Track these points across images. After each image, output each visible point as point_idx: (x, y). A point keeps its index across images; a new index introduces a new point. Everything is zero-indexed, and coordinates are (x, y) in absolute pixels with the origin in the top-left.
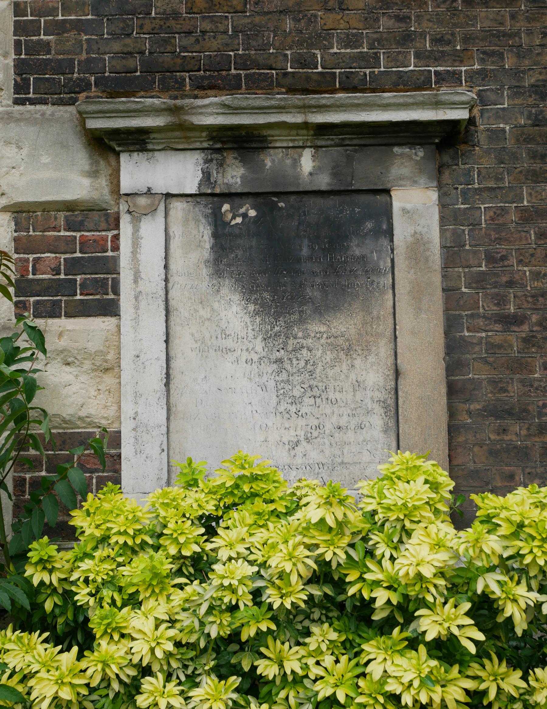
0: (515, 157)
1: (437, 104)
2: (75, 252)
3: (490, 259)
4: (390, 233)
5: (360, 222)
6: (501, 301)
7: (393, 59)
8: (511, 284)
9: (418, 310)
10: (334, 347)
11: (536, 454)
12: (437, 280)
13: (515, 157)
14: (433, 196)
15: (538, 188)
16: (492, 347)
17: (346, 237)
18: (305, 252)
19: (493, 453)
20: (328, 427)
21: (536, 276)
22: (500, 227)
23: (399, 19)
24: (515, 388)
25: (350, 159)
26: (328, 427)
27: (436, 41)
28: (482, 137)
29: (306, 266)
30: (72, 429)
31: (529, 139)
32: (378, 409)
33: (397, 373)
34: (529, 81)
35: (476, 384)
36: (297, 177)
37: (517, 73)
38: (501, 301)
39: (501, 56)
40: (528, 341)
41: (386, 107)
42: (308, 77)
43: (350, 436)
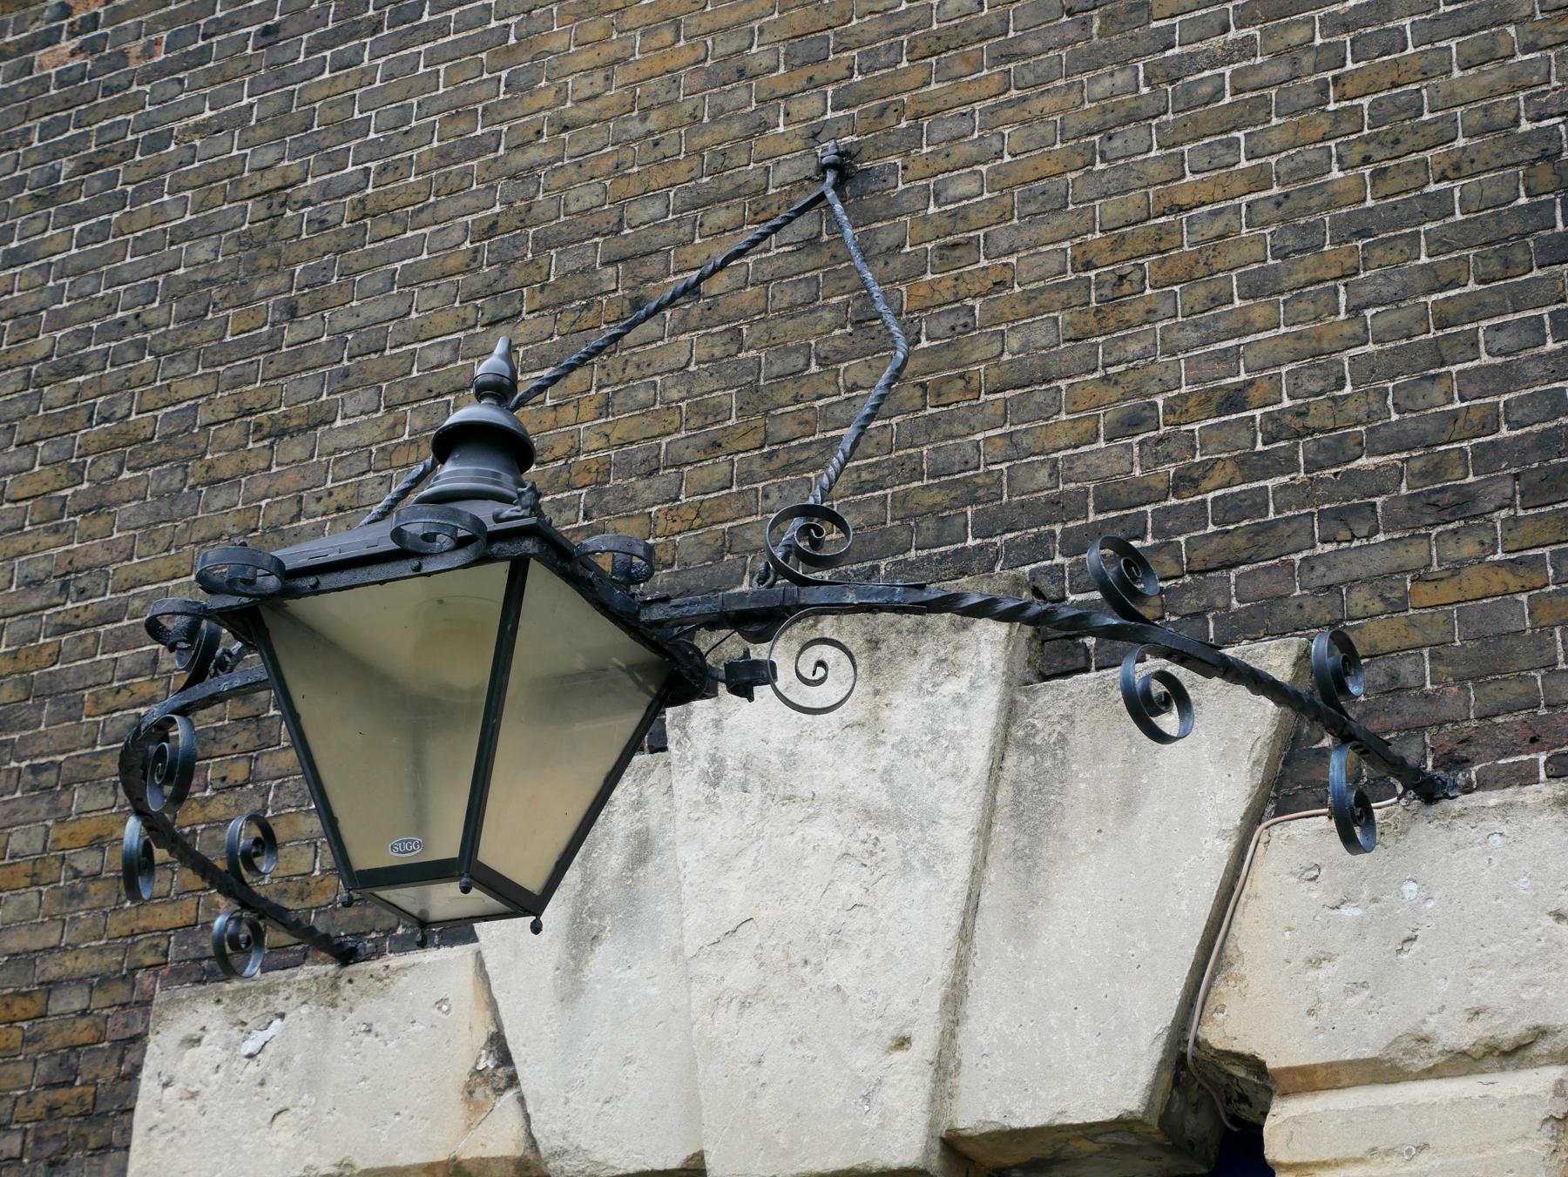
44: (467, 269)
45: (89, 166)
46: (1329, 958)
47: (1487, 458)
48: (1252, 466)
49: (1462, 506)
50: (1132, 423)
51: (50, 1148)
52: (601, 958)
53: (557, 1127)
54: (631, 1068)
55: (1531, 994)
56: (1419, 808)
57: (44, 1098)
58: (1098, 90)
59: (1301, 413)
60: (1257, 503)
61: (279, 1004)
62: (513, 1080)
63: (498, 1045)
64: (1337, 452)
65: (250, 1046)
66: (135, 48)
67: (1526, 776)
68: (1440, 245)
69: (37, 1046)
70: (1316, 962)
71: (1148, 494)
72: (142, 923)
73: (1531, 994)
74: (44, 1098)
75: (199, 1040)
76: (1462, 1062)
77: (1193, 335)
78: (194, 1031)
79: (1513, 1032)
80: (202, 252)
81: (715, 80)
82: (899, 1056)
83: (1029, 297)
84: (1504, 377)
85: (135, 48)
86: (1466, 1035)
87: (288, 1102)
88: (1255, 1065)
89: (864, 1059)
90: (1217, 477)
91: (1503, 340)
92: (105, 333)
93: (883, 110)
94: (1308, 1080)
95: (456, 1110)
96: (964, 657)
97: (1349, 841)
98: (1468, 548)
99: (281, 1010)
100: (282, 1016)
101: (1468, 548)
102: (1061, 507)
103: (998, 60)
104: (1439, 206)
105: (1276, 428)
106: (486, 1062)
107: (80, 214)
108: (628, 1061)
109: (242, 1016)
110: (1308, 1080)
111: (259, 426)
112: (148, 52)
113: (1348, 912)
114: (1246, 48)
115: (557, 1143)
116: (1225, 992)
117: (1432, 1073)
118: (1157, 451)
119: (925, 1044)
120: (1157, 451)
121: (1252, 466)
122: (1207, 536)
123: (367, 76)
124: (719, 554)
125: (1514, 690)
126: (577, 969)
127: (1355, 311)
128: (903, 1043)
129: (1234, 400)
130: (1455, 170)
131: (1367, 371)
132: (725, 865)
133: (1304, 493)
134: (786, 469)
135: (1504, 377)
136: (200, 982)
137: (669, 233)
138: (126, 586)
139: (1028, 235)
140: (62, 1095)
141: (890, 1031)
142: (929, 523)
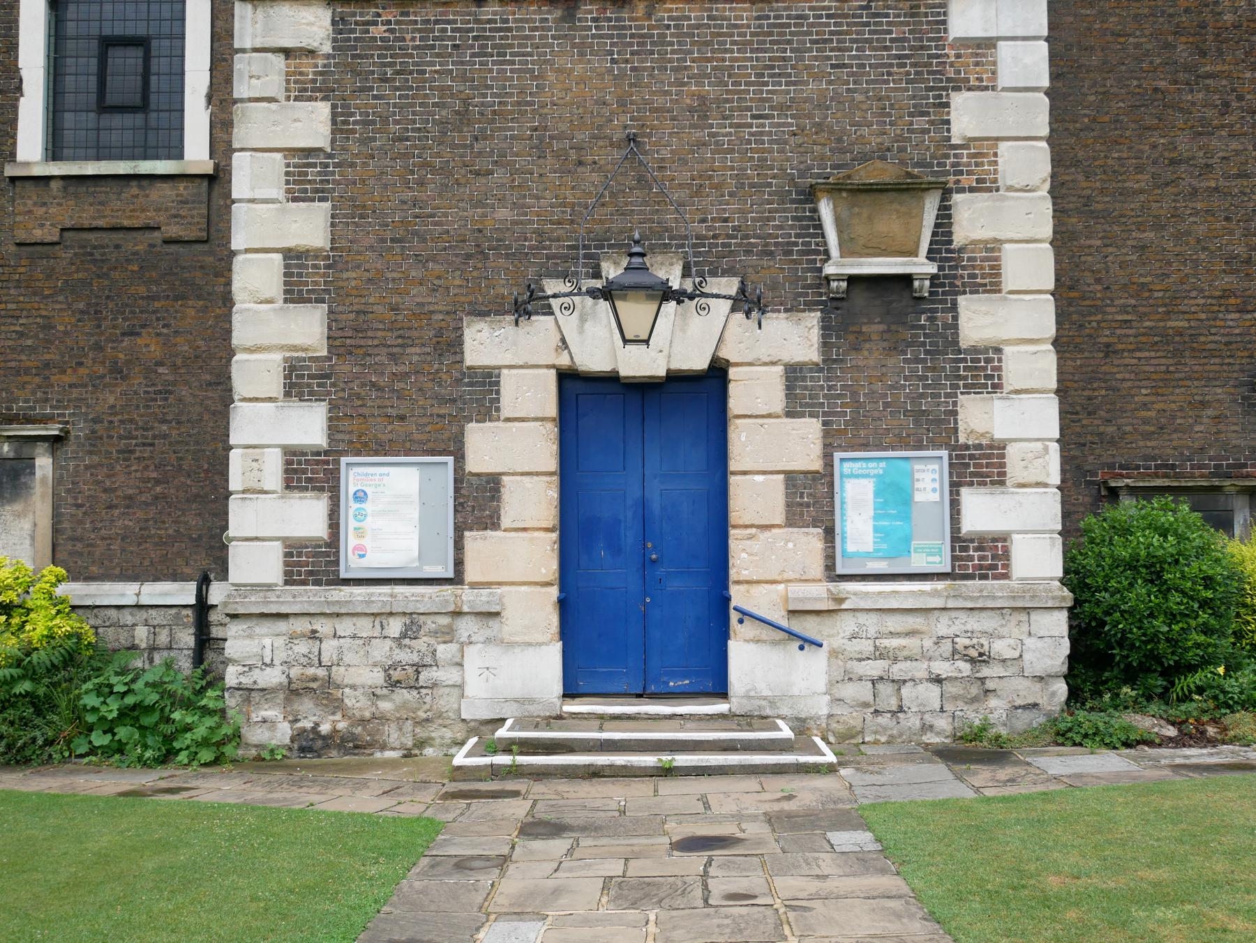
0: (84, 445)
1: (47, 429)
2: (914, 253)
3: (73, 483)
4: (34, 474)
5: (25, 469)
6: (76, 498)
7: (41, 408)
8: (80, 492)
9: (43, 502)
10: (14, 515)
11: (85, 555)
12: (51, 491)
13: (84, 445)
14: (51, 460)
15: (1158, 265)
16: (72, 515)
17: (20, 475)
18: (5, 480)
19: (70, 554)
20: (11, 544)
21: (89, 489)
22: (77, 472)
23: (44, 393)
24: (79, 530)
25: (21, 447)
26: (11, 544)
27: (57, 401)
28: (72, 438)
29: (5, 485)
30: (922, 593)
31: (89, 439)
32: (28, 537)
33: (35, 525)
34: (90, 417)
35: (65, 529)
36: (2, 453)
37: (86, 414)
38: (76, 498)
39: (81, 407)
40: (85, 513)
41: (29, 430)
42: (10, 414)
43: (18, 547)
44: (529, 139)
45: (398, 73)
47: (776, 244)
48: (729, 236)
49: (771, 254)
50: (704, 221)
51: (439, 352)
52: (588, 325)
56: (268, 16)
57: (435, 340)
58: (697, 135)
59: (740, 226)
60: (729, 245)
62: (567, 347)
63: (563, 340)
64: (747, 237)
65: (496, 334)
66: (408, 37)
67: (779, 311)
68: (770, 195)
71: (706, 238)
74: (435, 340)
76: (765, 364)
77: (716, 203)
79: (775, 360)
80: (444, 113)
81: (596, 102)
83: (680, 185)
84: (780, 227)
85: (408, 37)
86: (767, 360)
88: (727, 361)
90: (722, 237)
91: (781, 219)
92: (413, 130)
93: (643, 125)
94: (737, 365)
95: (553, 354)
96: (672, 272)
97: (748, 318)
98: (772, 263)
101: (772, 263)
102: (686, 237)
103: (671, 120)
104: (770, 185)
105: (734, 228)
106: (560, 344)
107: (398, 89)
110: (737, 365)
111: (471, 171)
112: (413, 39)
114: (730, 134)
116: (723, 346)
118: (708, 228)
119: (666, 352)
120: (708, 228)
121: (729, 236)
123: (491, 71)
124: (606, 233)
125: (778, 294)
127: (752, 205)
128: (661, 351)
129: (726, 220)
130: (774, 178)
131: (753, 219)
133: (740, 245)
134: (622, 214)
135: (780, 227)
136: (947, 800)
137: (587, 144)
139: (679, 169)
140: (440, 339)
142: (657, 235)
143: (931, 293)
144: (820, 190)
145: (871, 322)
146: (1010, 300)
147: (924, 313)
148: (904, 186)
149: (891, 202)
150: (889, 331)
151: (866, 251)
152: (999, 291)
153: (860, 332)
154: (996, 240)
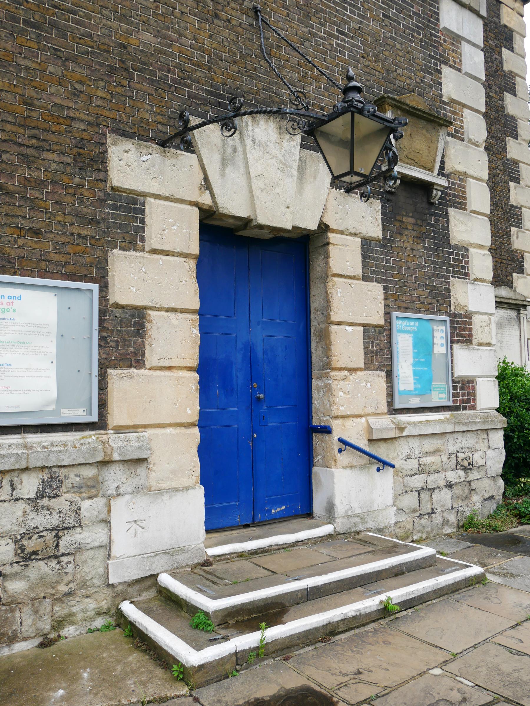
46: (338, 213)
52: (228, 170)
53: (222, 202)
54: (235, 195)
55: (360, 227)
61: (150, 150)
65: (144, 159)
69: (70, 134)
70: (336, 213)
72: (100, 112)
73: (360, 227)
75: (128, 152)
78: (127, 149)
82: (287, 209)
86: (353, 231)
87: (156, 176)
89: (283, 208)
94: (334, 231)
99: (151, 153)
100: (151, 154)
108: (235, 193)
109: (141, 150)
113: (340, 206)
115: (222, 205)
117: (347, 235)
122: (138, 71)
126: (223, 170)
132: (257, 161)
138: (77, 5)
141: (287, 205)
143: (440, 203)
144: (388, 104)
145: (407, 216)
146: (473, 216)
147: (433, 215)
148: (432, 118)
149: (423, 128)
150: (416, 224)
151: (407, 160)
152: (465, 209)
153: (402, 221)
154: (466, 174)
